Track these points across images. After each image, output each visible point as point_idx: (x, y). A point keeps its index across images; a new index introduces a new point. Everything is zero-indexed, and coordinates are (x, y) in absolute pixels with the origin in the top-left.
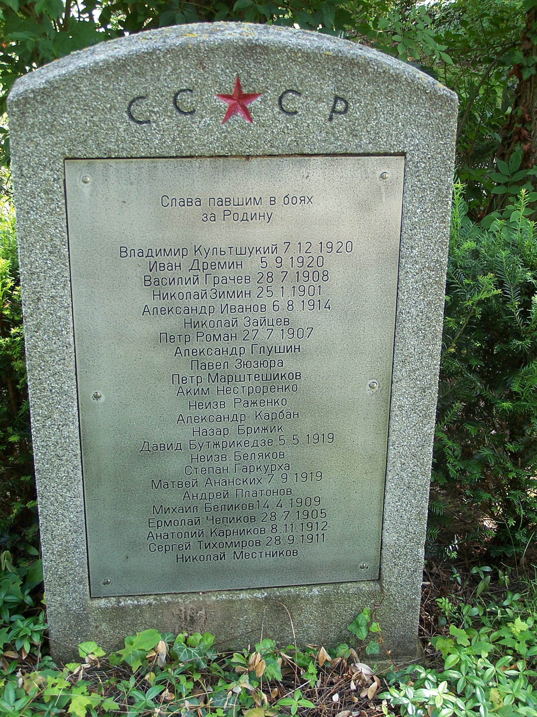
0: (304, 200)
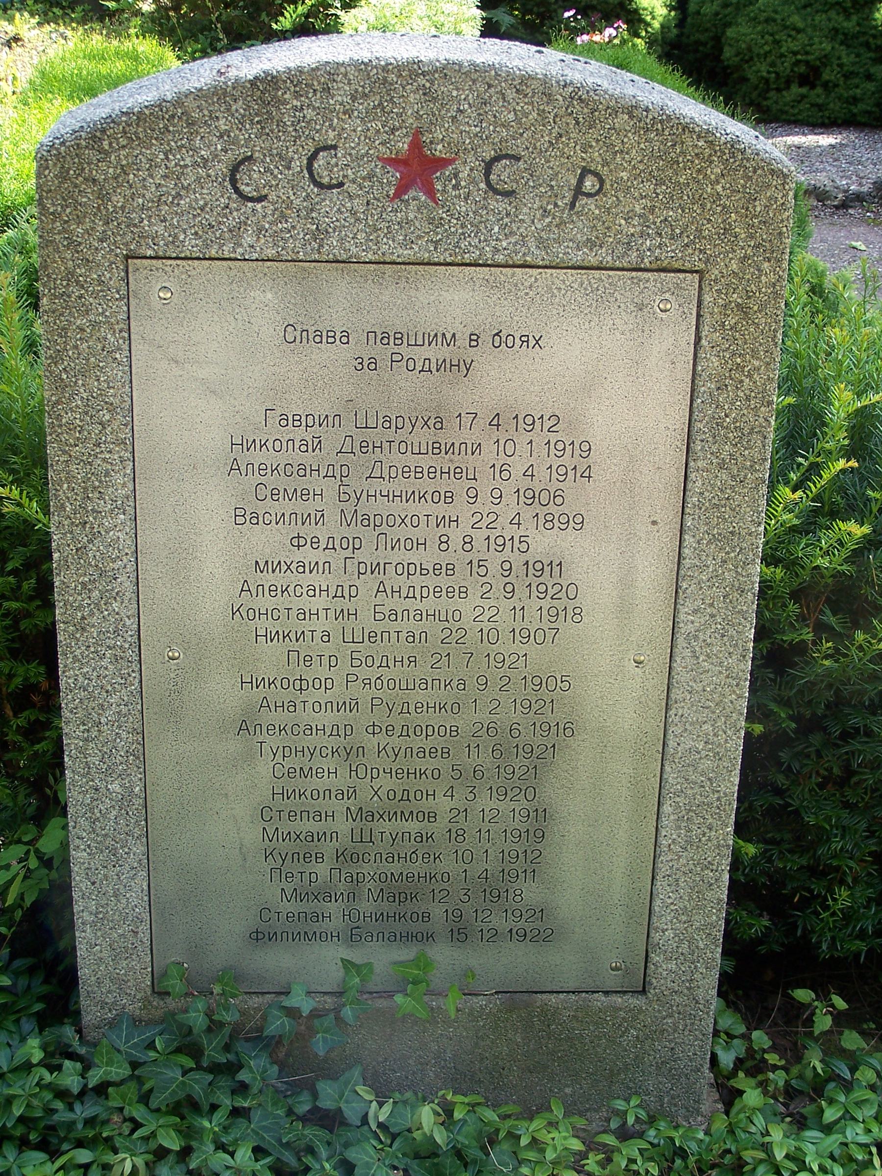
0: (527, 341)
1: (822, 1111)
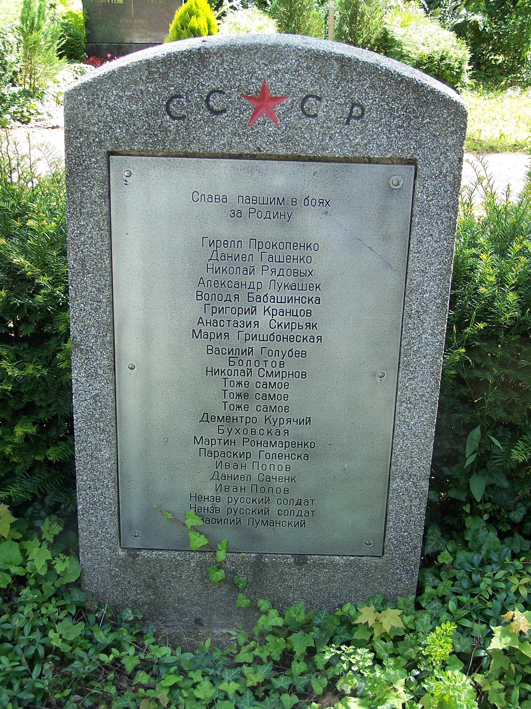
0: (323, 203)
1: (491, 635)
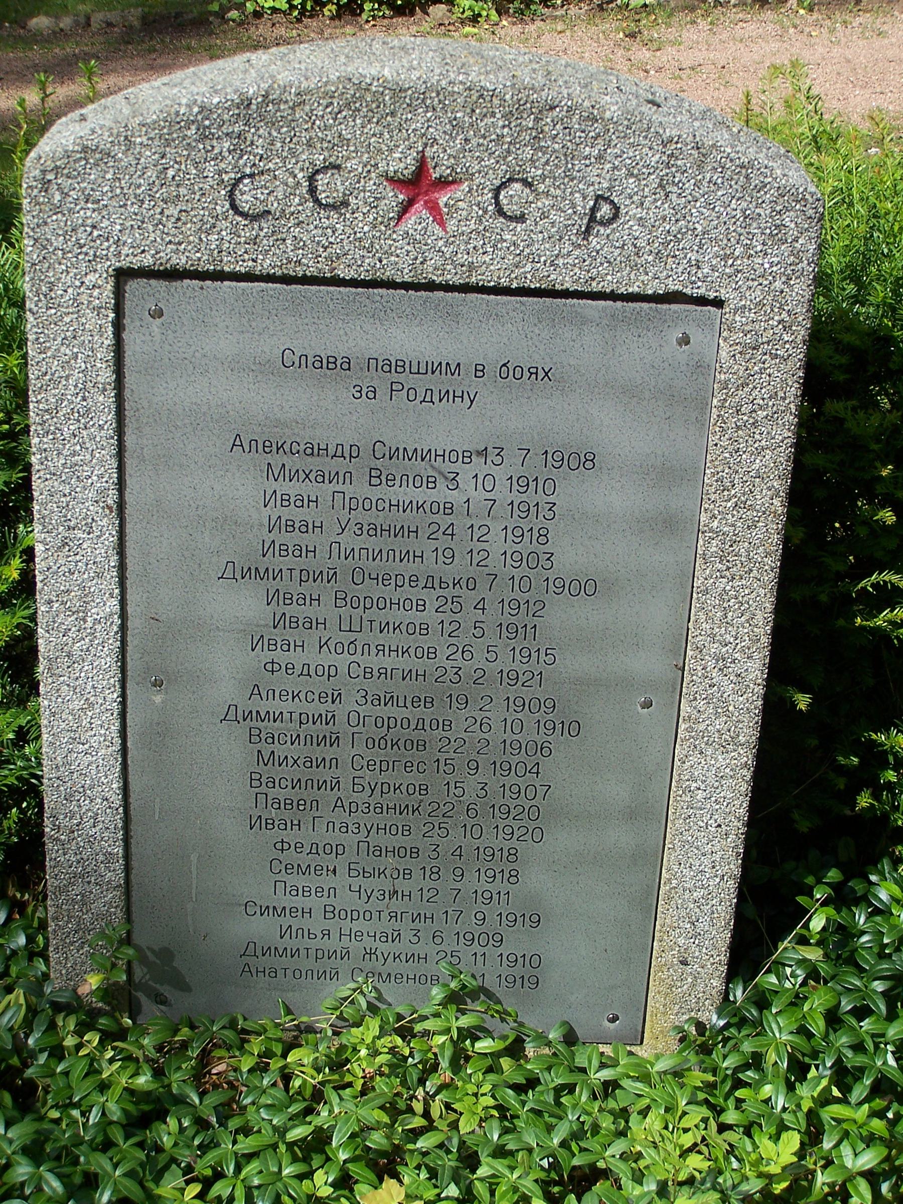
0: (536, 373)
